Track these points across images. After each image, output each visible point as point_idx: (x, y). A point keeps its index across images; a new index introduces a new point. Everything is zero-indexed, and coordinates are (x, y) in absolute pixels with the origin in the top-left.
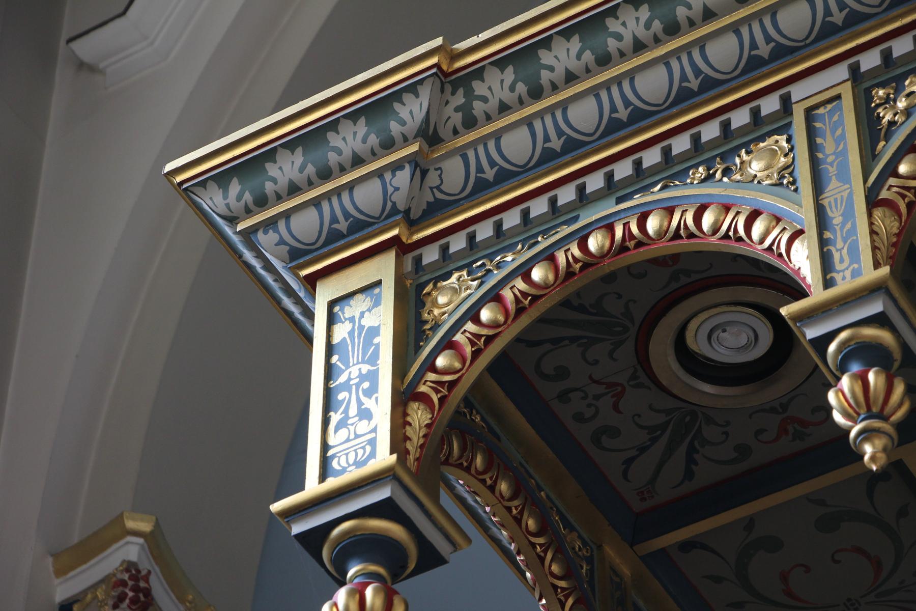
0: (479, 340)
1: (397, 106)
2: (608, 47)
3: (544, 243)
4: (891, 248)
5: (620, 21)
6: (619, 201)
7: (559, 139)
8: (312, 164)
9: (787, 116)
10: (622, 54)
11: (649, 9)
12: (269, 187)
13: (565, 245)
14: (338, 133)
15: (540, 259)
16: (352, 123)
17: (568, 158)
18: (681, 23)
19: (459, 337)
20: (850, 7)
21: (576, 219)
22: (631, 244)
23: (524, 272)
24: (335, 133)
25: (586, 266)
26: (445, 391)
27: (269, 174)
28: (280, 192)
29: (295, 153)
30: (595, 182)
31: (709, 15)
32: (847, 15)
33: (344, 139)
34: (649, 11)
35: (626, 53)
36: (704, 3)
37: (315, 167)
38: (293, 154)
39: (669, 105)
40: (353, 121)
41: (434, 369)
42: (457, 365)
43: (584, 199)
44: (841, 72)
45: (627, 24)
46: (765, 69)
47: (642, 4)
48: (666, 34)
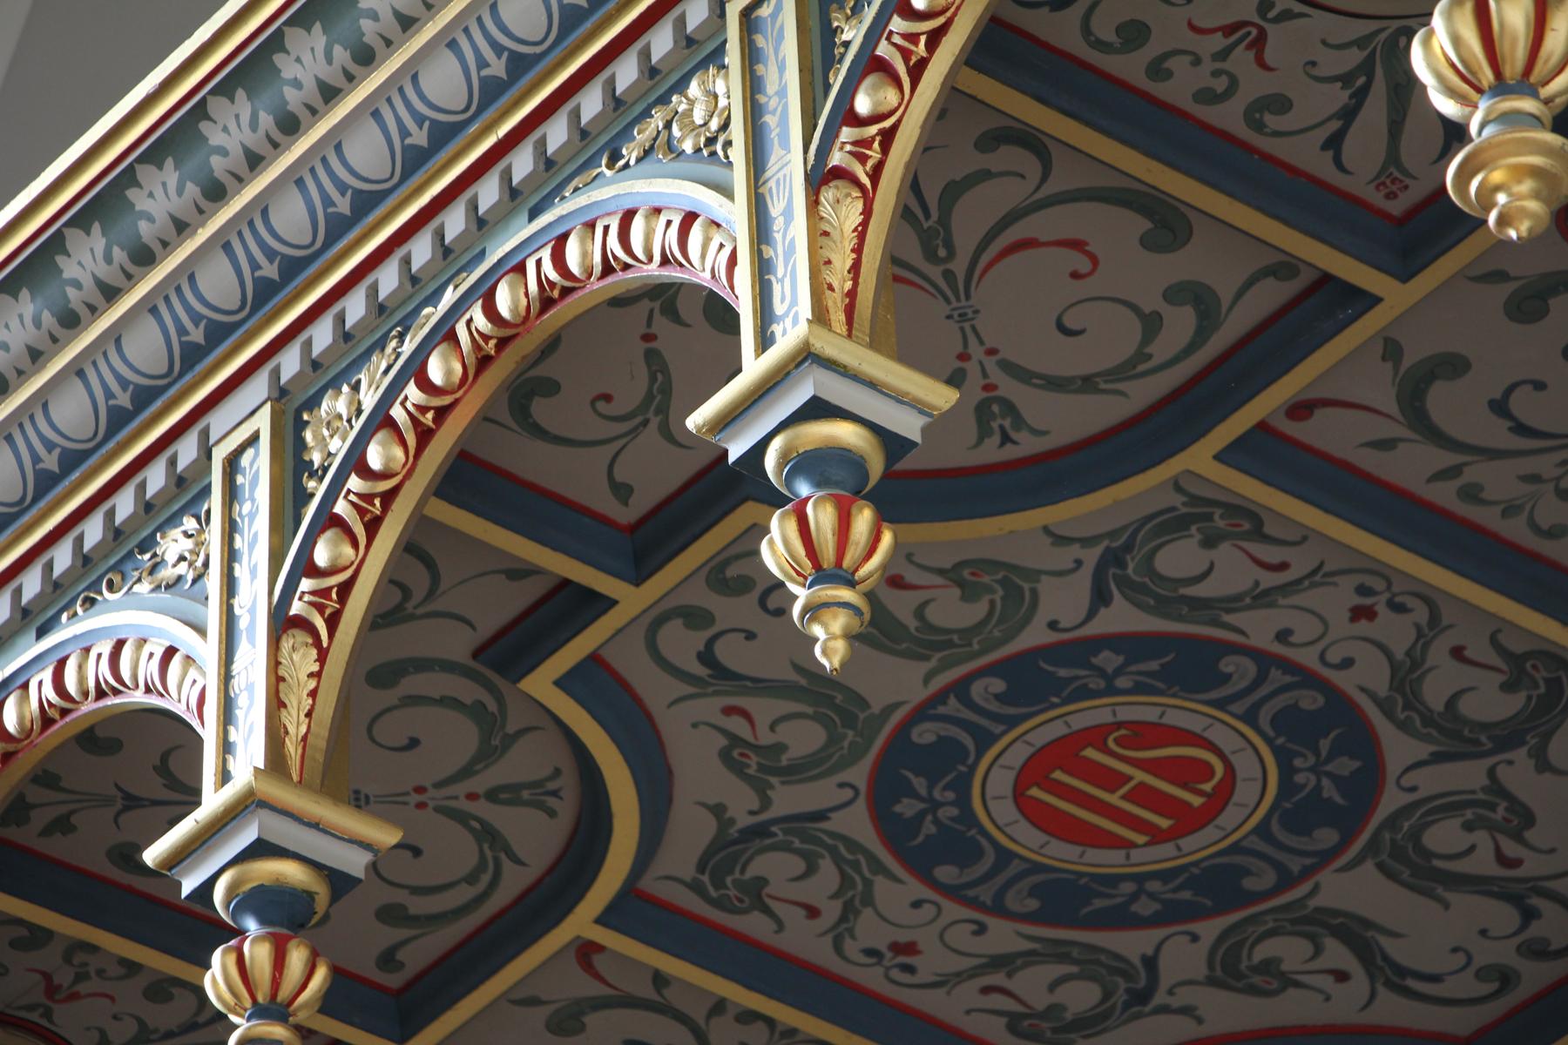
0: (916, 43)
1: (132, 194)
2: (363, 35)
3: (433, 315)
4: (845, 299)
5: (293, 56)
6: (534, 214)
7: (421, 128)
8: (192, 182)
9: (384, 321)
10: (93, 309)
11: (248, 96)
12: (293, 97)
13: (464, 313)
14: (288, 53)
15: (436, 341)
16: (81, 233)
17: (443, 156)
18: (77, 310)
19: (341, 507)
20: (60, 446)
21: (482, 255)
22: (52, 713)
23: (416, 370)
24: (227, 100)
25: (502, 343)
26: (332, 605)
27: (138, 208)
28: (178, 215)
29: (19, 297)
30: (488, 192)
31: (408, 23)
32: (206, 328)
33: (298, 60)
34: (175, 170)
35: (187, 221)
36: (316, 77)
37: (197, 185)
38: (233, 102)
39: (557, 36)
40: (156, 165)
41: (313, 571)
42: (348, 551)
43: (482, 225)
44: (258, 388)
45: (303, 59)
46: (432, 165)
47: (20, 290)
48: (359, 64)
